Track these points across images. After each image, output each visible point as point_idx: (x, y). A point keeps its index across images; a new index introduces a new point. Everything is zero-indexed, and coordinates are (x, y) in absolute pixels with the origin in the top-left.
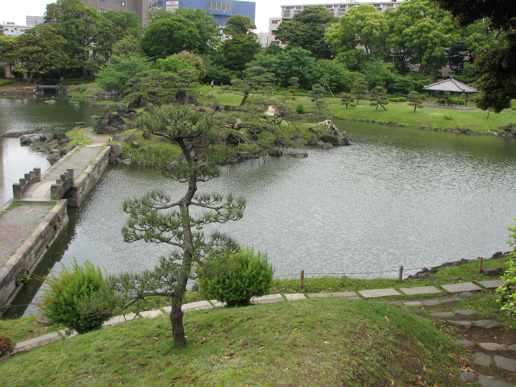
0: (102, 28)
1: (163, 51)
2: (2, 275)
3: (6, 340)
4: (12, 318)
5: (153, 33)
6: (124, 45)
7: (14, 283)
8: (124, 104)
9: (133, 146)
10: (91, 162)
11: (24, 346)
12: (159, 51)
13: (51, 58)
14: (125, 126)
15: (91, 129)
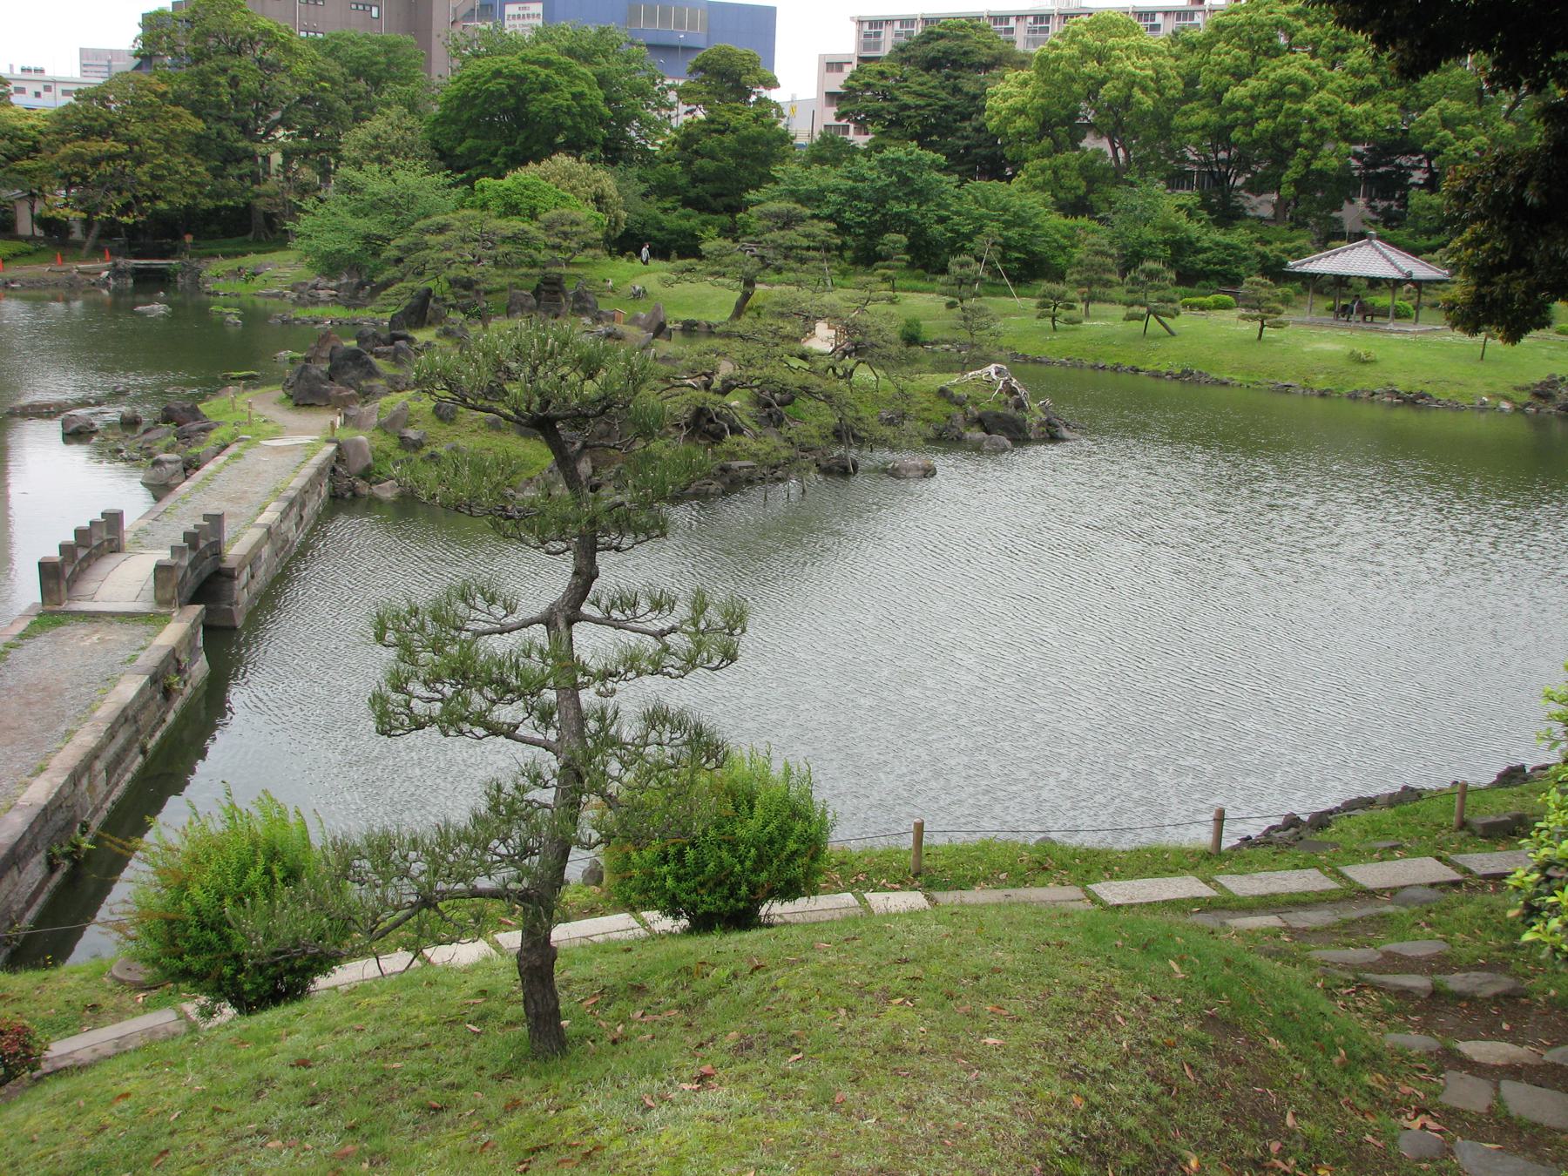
0: (311, 84)
1: (494, 154)
2: (5, 834)
3: (19, 1033)
4: (36, 967)
5: (465, 100)
6: (376, 137)
7: (43, 861)
8: (377, 315)
9: (405, 443)
10: (276, 493)
11: (72, 1052)
12: (482, 156)
13: (154, 177)
14: (379, 383)
15: (277, 392)
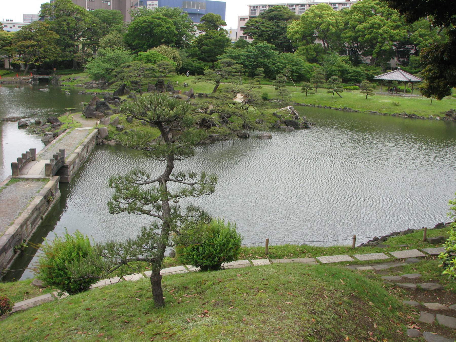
1: (144, 45)
3: (5, 301)
4: (10, 281)
5: (135, 29)
6: (109, 40)
7: (13, 250)
8: (110, 91)
10: (80, 143)
11: (21, 306)
12: (140, 45)
13: (45, 51)
14: (110, 111)
15: (81, 114)
